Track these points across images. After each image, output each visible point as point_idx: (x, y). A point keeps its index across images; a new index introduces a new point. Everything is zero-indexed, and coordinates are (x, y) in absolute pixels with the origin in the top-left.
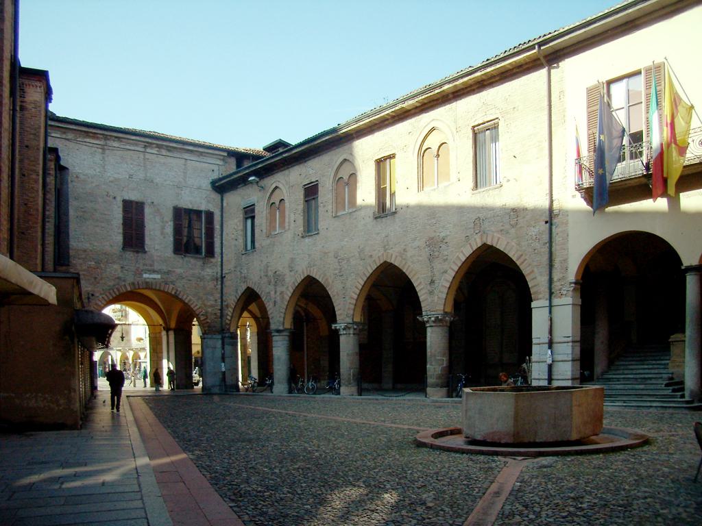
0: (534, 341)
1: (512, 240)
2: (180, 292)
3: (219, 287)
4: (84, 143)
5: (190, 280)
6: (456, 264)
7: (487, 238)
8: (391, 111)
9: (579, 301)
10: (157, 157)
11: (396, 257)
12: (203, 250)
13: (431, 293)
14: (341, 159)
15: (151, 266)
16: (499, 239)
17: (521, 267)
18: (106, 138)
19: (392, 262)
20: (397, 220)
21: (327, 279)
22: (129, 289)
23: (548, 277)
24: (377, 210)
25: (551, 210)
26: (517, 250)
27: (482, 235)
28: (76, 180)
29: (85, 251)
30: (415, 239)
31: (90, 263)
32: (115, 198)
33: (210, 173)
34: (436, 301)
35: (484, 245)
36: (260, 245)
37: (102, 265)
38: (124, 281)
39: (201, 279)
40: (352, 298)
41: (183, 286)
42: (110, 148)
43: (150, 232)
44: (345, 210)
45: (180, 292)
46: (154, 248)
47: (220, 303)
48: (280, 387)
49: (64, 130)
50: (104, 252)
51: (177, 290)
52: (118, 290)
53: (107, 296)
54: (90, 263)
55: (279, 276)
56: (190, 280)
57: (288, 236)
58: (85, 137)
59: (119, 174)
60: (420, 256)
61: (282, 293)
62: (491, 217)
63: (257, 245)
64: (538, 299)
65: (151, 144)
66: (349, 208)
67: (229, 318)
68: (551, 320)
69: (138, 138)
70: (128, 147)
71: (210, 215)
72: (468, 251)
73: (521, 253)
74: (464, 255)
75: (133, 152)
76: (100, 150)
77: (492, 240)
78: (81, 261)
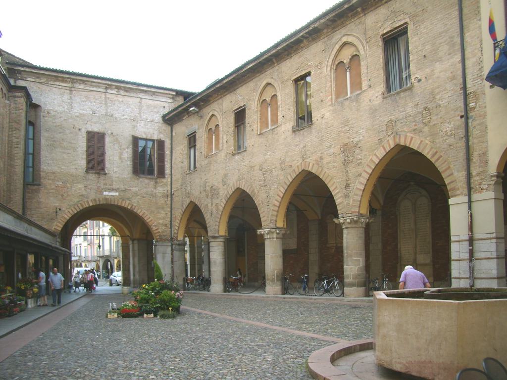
0: (453, 239)
1: (426, 138)
2: (135, 207)
3: (169, 202)
4: (55, 86)
5: (144, 197)
6: (370, 167)
7: (400, 140)
8: (304, 32)
9: (502, 196)
10: (117, 97)
11: (314, 164)
12: (156, 172)
13: (346, 196)
14: (264, 83)
15: (110, 185)
16: (412, 138)
17: (437, 165)
18: (73, 81)
19: (310, 169)
20: (313, 131)
21: (253, 191)
22: (91, 205)
23: (466, 173)
24: (295, 125)
25: (498, 278)
26: (432, 148)
27: (394, 137)
28: (47, 115)
29: (54, 173)
30: (330, 147)
31: (57, 183)
32: (80, 130)
33: (162, 109)
34: (351, 204)
35: (397, 146)
36: (200, 165)
37: (68, 185)
38: (87, 198)
39: (153, 195)
40: (274, 205)
41: (138, 202)
42: (76, 89)
43: (110, 157)
44: (268, 128)
45: (135, 207)
46: (113, 170)
47: (170, 216)
48: (217, 287)
49: (37, 75)
50: (70, 174)
51: (133, 205)
52: (82, 205)
53: (73, 211)
54: (57, 183)
55: (215, 190)
56: (144, 197)
57: (222, 155)
58: (55, 81)
59: (83, 110)
60: (335, 162)
61: (217, 205)
62: (403, 118)
63: (198, 165)
64: (455, 196)
65: (111, 85)
66: (272, 126)
67: (177, 228)
68: (471, 216)
69: (99, 81)
70: (91, 89)
71: (161, 144)
72: (381, 153)
73: (435, 151)
74: (377, 157)
75: (96, 92)
76: (68, 91)
77: (405, 141)
78: (50, 181)
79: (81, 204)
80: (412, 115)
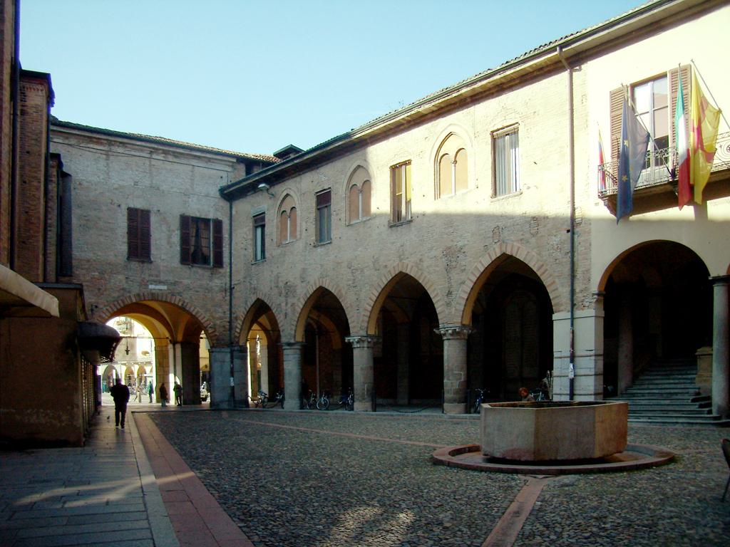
0: (556, 355)
1: (532, 249)
2: (187, 303)
3: (228, 298)
4: (88, 149)
5: (197, 292)
6: (474, 275)
7: (506, 248)
8: (406, 115)
9: (602, 313)
10: (164, 163)
11: (412, 267)
12: (212, 260)
13: (448, 304)
14: (354, 166)
15: (157, 276)
16: (519, 248)
17: (542, 278)
18: (110, 143)
19: (408, 272)
20: (413, 229)
21: (340, 291)
22: (134, 301)
23: (570, 289)
24: (392, 219)
25: (573, 218)
26: (538, 260)
27: (501, 245)
28: (79, 187)
29: (88, 261)
30: (431, 249)
31: (93, 274)
32: (119, 206)
33: (219, 180)
34: (453, 313)
35: (504, 255)
36: (271, 254)
37: (106, 276)
38: (129, 292)
39: (209, 290)
40: (366, 310)
41: (191, 297)
42: (115, 154)
43: (156, 241)
44: (359, 218)
45: (187, 303)
46: (160, 258)
47: (229, 315)
48: (291, 403)
49: (66, 135)
50: (108, 262)
51: (184, 302)
52: (123, 302)
53: (112, 308)
54: (93, 274)
55: (290, 287)
56: (197, 292)
57: (300, 245)
58: (88, 143)
59: (123, 181)
60: (437, 266)
61: (293, 305)
62: (510, 226)
63: (267, 254)
64: (559, 311)
65: (157, 149)
66: (363, 216)
67: (238, 330)
68: (573, 332)
69: (143, 144)
70: (133, 153)
71: (218, 224)
72: (487, 261)
73: (541, 263)
74: (482, 265)
75: (138, 158)
76: (104, 156)
77: (512, 249)
78: (84, 271)
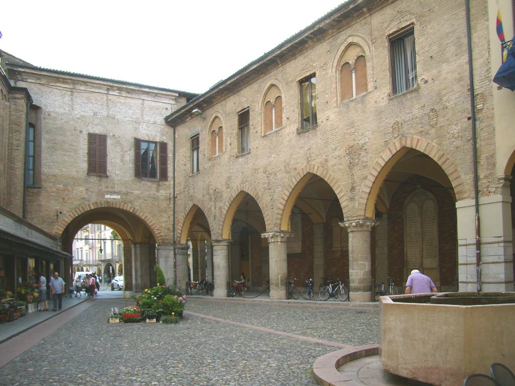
0: (460, 242)
1: (433, 140)
2: (137, 210)
3: (172, 206)
4: (56, 87)
5: (146, 200)
6: (376, 170)
7: (406, 142)
8: (309, 33)
9: (510, 199)
10: (119, 98)
11: (318, 167)
12: (158, 175)
13: (352, 199)
14: (268, 84)
15: (112, 188)
16: (418, 140)
17: (444, 167)
18: (74, 83)
19: (315, 172)
20: (318, 133)
21: (257, 194)
22: (93, 208)
23: (473, 176)
24: (300, 127)
25: (506, 282)
26: (439, 150)
27: (400, 139)
28: (48, 117)
29: (55, 176)
30: (335, 149)
31: (58, 186)
32: (81, 132)
33: (165, 110)
34: (356, 207)
35: (404, 148)
36: (203, 167)
37: (69, 188)
38: (89, 201)
39: (156, 199)
40: (279, 208)
41: (140, 205)
42: (77, 91)
43: (111, 160)
44: (272, 130)
45: (137, 210)
46: (115, 173)
47: (173, 220)
48: (220, 291)
49: (38, 77)
50: (71, 176)
51: (135, 209)
52: (83, 209)
53: (74, 214)
54: (58, 186)
55: (218, 193)
56: (146, 200)
57: (226, 157)
58: (56, 82)
59: (84, 112)
60: (341, 164)
61: (220, 208)
62: (409, 120)
63: (201, 168)
64: (462, 199)
65: (112, 87)
66: (276, 128)
67: (179, 231)
68: (479, 219)
69: (101, 82)
70: (93, 90)
71: (163, 146)
72: (387, 156)
73: (442, 153)
74: (383, 159)
75: (97, 94)
76: (69, 93)
77: (411, 143)
78: (51, 184)
79: (82, 207)
80: (418, 117)
